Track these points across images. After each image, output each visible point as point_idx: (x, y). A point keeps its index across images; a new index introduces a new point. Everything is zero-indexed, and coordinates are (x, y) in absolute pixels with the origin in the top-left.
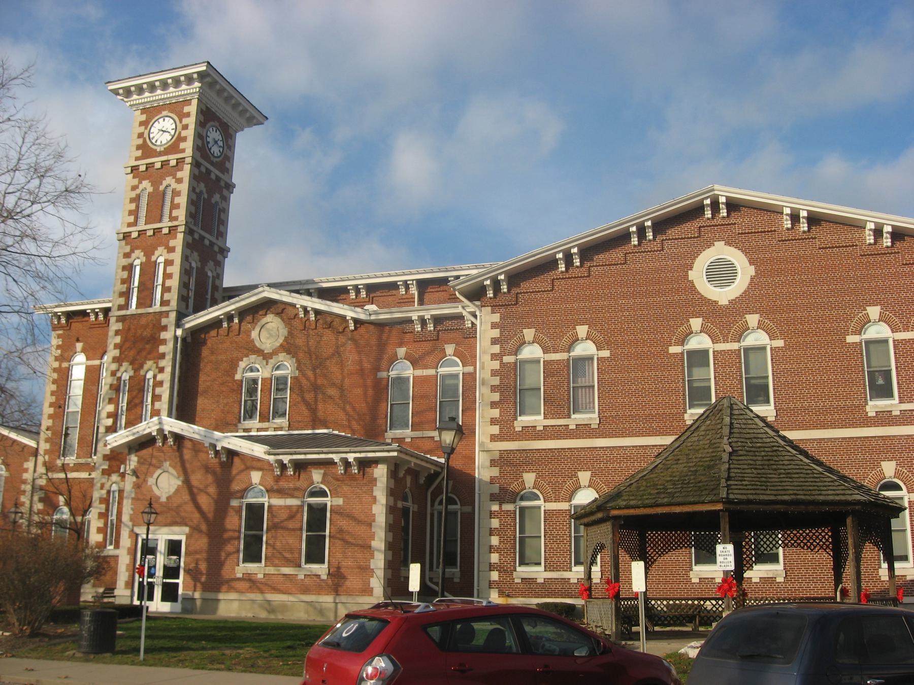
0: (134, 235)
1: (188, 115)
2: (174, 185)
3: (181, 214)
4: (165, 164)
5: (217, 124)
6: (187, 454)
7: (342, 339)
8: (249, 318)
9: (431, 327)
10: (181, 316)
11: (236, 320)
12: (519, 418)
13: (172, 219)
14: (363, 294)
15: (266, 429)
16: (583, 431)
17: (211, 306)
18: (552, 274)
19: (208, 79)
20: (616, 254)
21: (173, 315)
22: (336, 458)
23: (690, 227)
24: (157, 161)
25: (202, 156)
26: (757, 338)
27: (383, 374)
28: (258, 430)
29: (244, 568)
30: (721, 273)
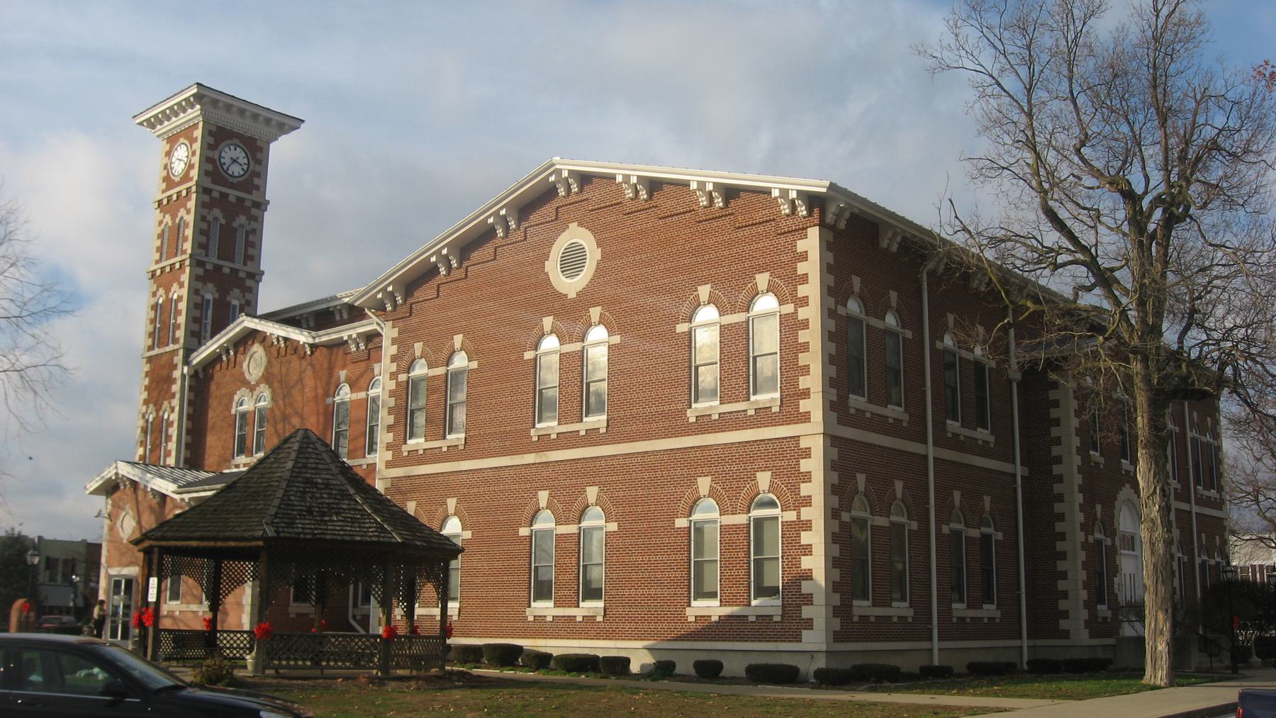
4: (179, 193)
6: (140, 493)
7: (304, 363)
10: (188, 352)
11: (232, 353)
12: (409, 442)
16: (592, 438)
18: (437, 281)
19: (206, 100)
20: (487, 250)
21: (181, 352)
23: (548, 210)
25: (214, 182)
27: (329, 400)
30: (572, 261)
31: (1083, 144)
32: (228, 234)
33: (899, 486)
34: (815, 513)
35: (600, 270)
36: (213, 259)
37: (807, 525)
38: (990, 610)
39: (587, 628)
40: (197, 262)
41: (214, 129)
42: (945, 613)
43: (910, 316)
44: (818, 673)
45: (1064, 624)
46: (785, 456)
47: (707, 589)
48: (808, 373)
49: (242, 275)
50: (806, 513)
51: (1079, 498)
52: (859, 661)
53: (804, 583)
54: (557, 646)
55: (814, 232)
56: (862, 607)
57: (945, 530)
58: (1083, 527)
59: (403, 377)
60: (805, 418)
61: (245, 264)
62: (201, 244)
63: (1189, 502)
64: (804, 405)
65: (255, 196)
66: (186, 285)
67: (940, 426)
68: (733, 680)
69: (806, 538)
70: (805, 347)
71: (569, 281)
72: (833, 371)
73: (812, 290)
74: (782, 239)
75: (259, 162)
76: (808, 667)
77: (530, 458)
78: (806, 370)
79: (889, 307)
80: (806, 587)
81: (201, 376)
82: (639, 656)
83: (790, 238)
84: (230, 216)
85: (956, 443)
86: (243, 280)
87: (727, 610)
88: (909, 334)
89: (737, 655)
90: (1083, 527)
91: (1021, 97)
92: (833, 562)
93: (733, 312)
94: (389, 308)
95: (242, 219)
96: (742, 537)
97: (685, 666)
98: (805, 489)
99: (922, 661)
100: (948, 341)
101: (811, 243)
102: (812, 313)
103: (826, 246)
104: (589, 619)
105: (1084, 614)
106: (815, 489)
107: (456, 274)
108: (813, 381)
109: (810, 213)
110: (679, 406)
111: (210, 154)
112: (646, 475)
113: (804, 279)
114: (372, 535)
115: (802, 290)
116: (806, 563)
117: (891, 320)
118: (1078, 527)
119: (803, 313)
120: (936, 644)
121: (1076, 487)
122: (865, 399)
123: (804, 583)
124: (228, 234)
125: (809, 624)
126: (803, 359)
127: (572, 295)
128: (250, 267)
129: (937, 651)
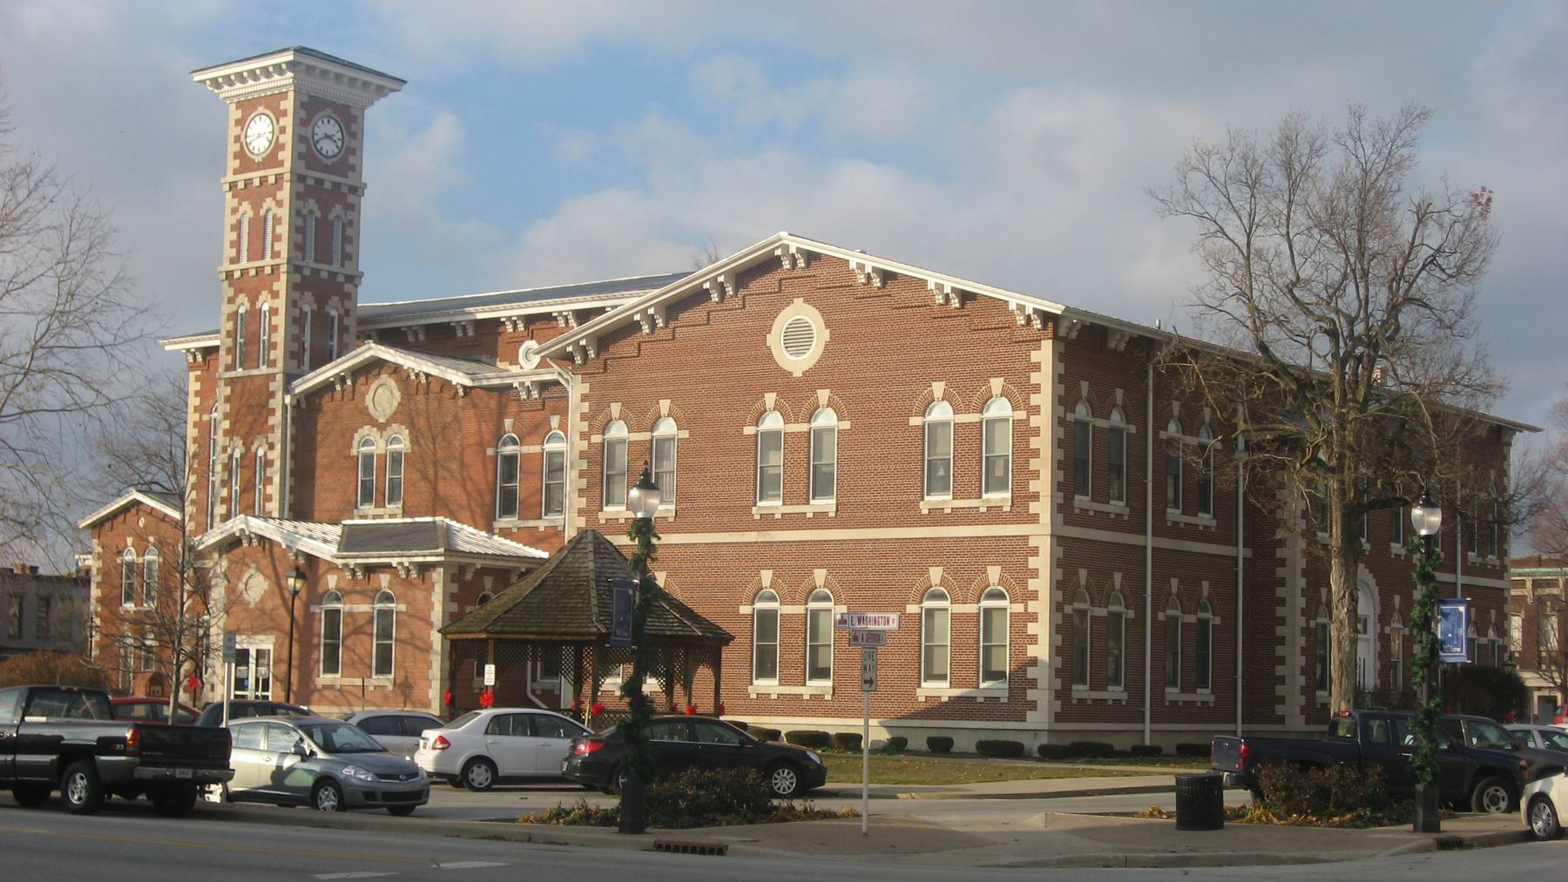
0: (237, 275)
1: (284, 113)
2: (275, 210)
3: (283, 247)
4: (263, 180)
5: (329, 111)
8: (362, 379)
9: (535, 394)
10: (290, 378)
11: (349, 382)
13: (275, 255)
14: (521, 327)
15: (381, 517)
16: (820, 520)
17: (339, 356)
20: (698, 313)
21: (280, 377)
22: (394, 562)
23: (769, 281)
24: (255, 176)
26: (827, 419)
28: (374, 517)
29: (324, 678)
30: (798, 338)
31: (1295, 285)
32: (324, 228)
33: (1118, 577)
34: (1041, 607)
35: (828, 350)
36: (310, 262)
37: (1034, 618)
38: (1204, 694)
39: (816, 705)
40: (294, 268)
41: (306, 99)
42: (1158, 697)
43: (1135, 412)
44: (1042, 749)
45: (1279, 709)
46: (1015, 554)
47: (936, 671)
48: (1038, 477)
49: (340, 279)
50: (1033, 606)
51: (1302, 582)
52: (1076, 739)
53: (1029, 669)
54: (785, 724)
55: (1047, 345)
56: (1080, 691)
57: (1161, 616)
58: (1304, 612)
59: (596, 439)
60: (1034, 519)
61: (342, 265)
62: (297, 247)
63: (1454, 571)
64: (1033, 507)
65: (351, 180)
66: (283, 294)
67: (1159, 514)
68: (964, 755)
69: (1032, 628)
70: (1036, 453)
71: (793, 358)
72: (1061, 475)
73: (1044, 400)
74: (1017, 347)
75: (353, 135)
76: (1032, 744)
77: (752, 537)
78: (1036, 475)
79: (1115, 405)
80: (1031, 673)
81: (304, 405)
82: (877, 733)
83: (1024, 347)
84: (325, 208)
85: (1176, 531)
86: (342, 284)
87: (957, 692)
88: (1133, 429)
89: (967, 734)
90: (1304, 612)
91: (1241, 240)
92: (1056, 651)
93: (967, 411)
94: (578, 360)
95: (338, 209)
96: (972, 625)
97: (918, 742)
98: (1032, 584)
99: (1134, 741)
100: (1173, 429)
101: (1044, 355)
102: (1043, 421)
103: (1060, 357)
104: (817, 697)
105: (1302, 700)
106: (1041, 584)
107: (660, 334)
108: (1043, 485)
109: (1045, 327)
110: (912, 498)
111: (303, 131)
112: (877, 562)
113: (1037, 389)
114: (677, 629)
115: (1035, 399)
116: (1032, 651)
117: (1116, 418)
118: (1298, 612)
119: (1034, 421)
120: (1148, 726)
121: (1299, 571)
122: (1088, 498)
123: (1029, 669)
124: (324, 228)
125: (1033, 705)
126: (1034, 443)
127: (798, 374)
128: (348, 270)
129: (1148, 731)
